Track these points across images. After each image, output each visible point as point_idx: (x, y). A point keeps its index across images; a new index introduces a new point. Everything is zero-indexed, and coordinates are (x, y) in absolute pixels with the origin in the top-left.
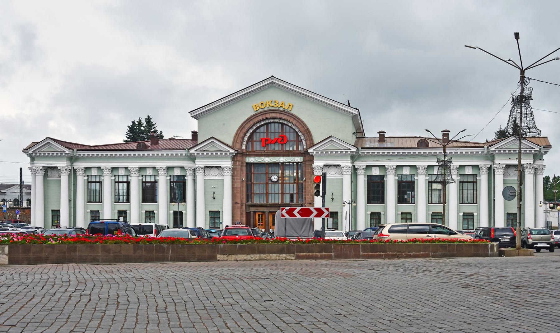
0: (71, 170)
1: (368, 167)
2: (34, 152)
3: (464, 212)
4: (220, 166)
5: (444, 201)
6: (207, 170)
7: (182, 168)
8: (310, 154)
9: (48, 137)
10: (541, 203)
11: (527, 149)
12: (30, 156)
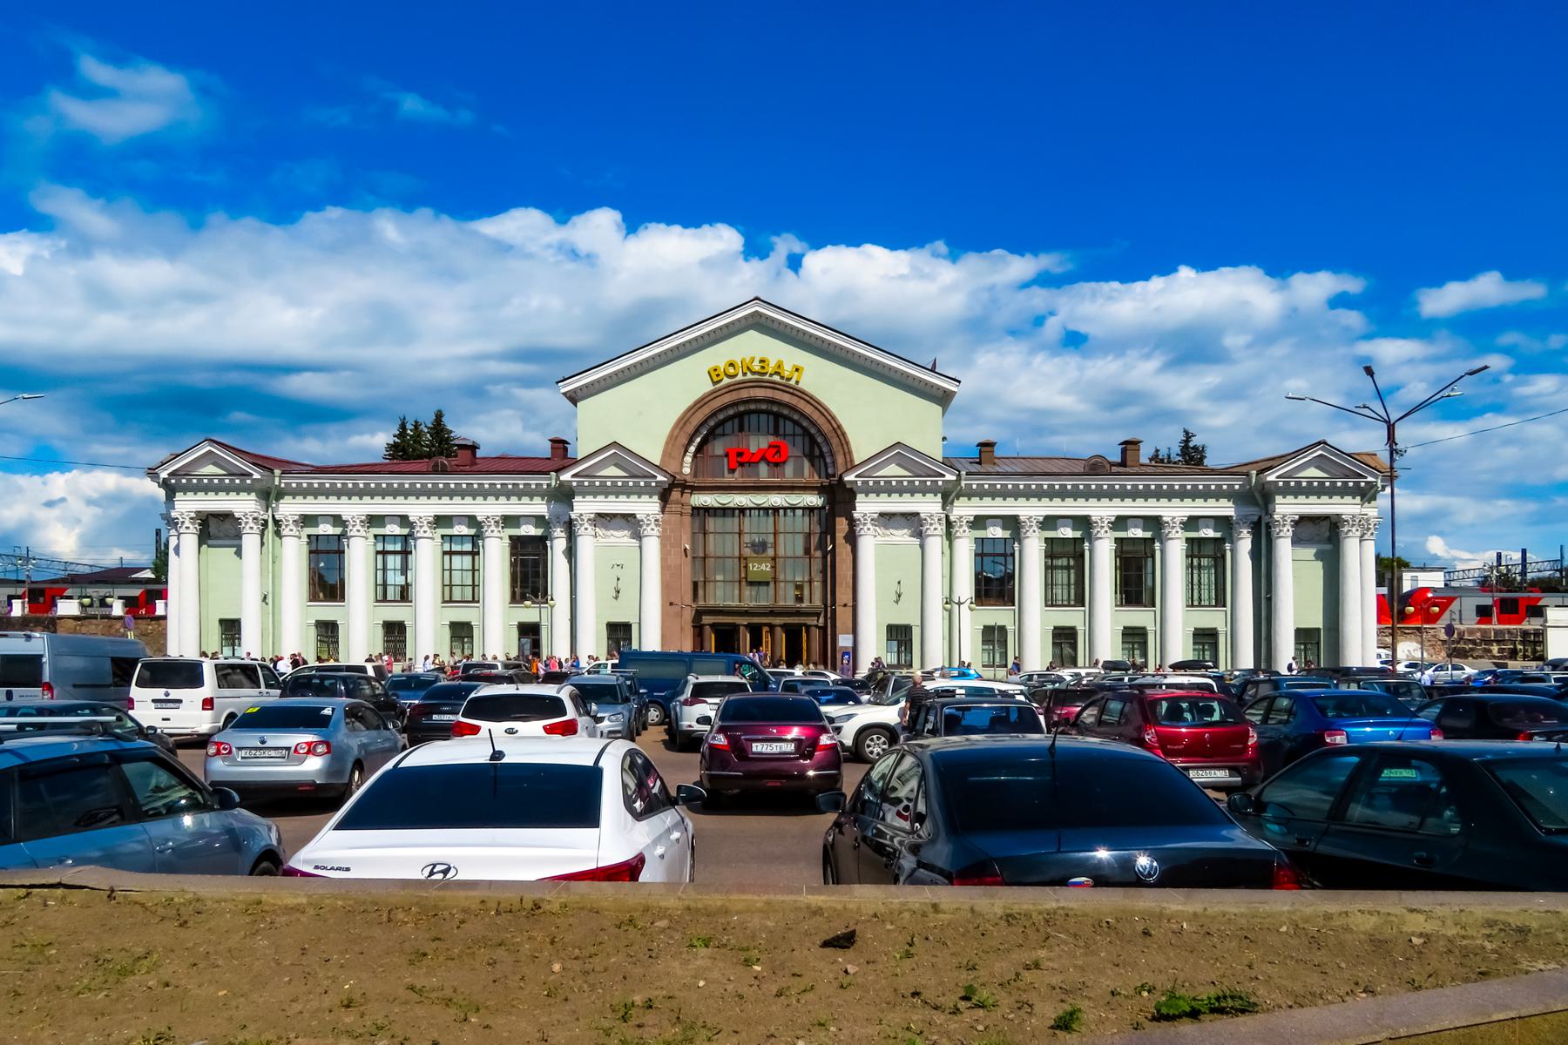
2: (172, 474)
3: (987, 624)
4: (634, 514)
8: (848, 486)
11: (1347, 477)
12: (165, 484)
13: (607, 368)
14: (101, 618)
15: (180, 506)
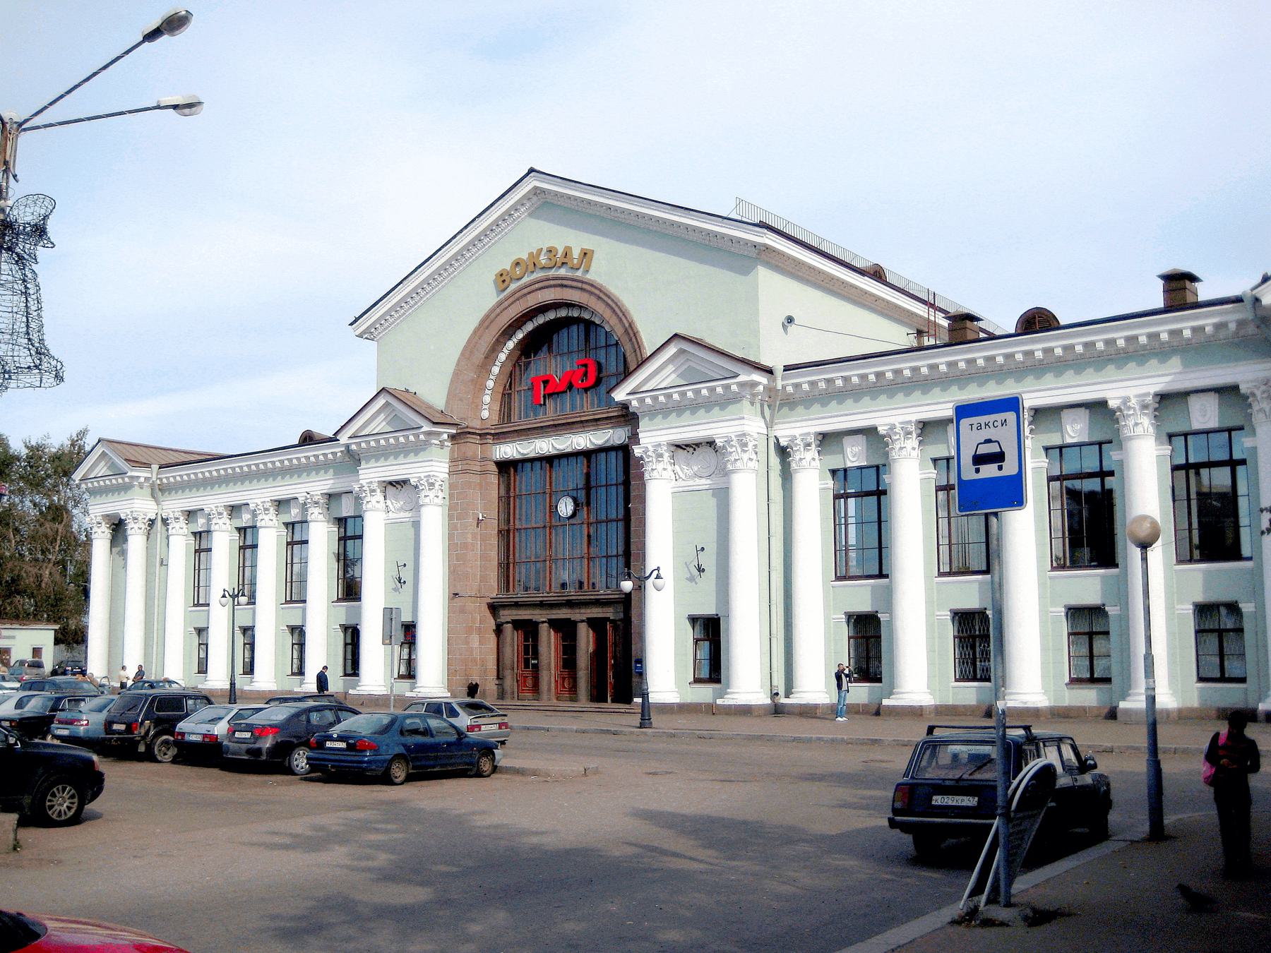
0: (152, 523)
1: (1164, 399)
9: (678, 331)
10: (224, 596)
13: (738, 229)
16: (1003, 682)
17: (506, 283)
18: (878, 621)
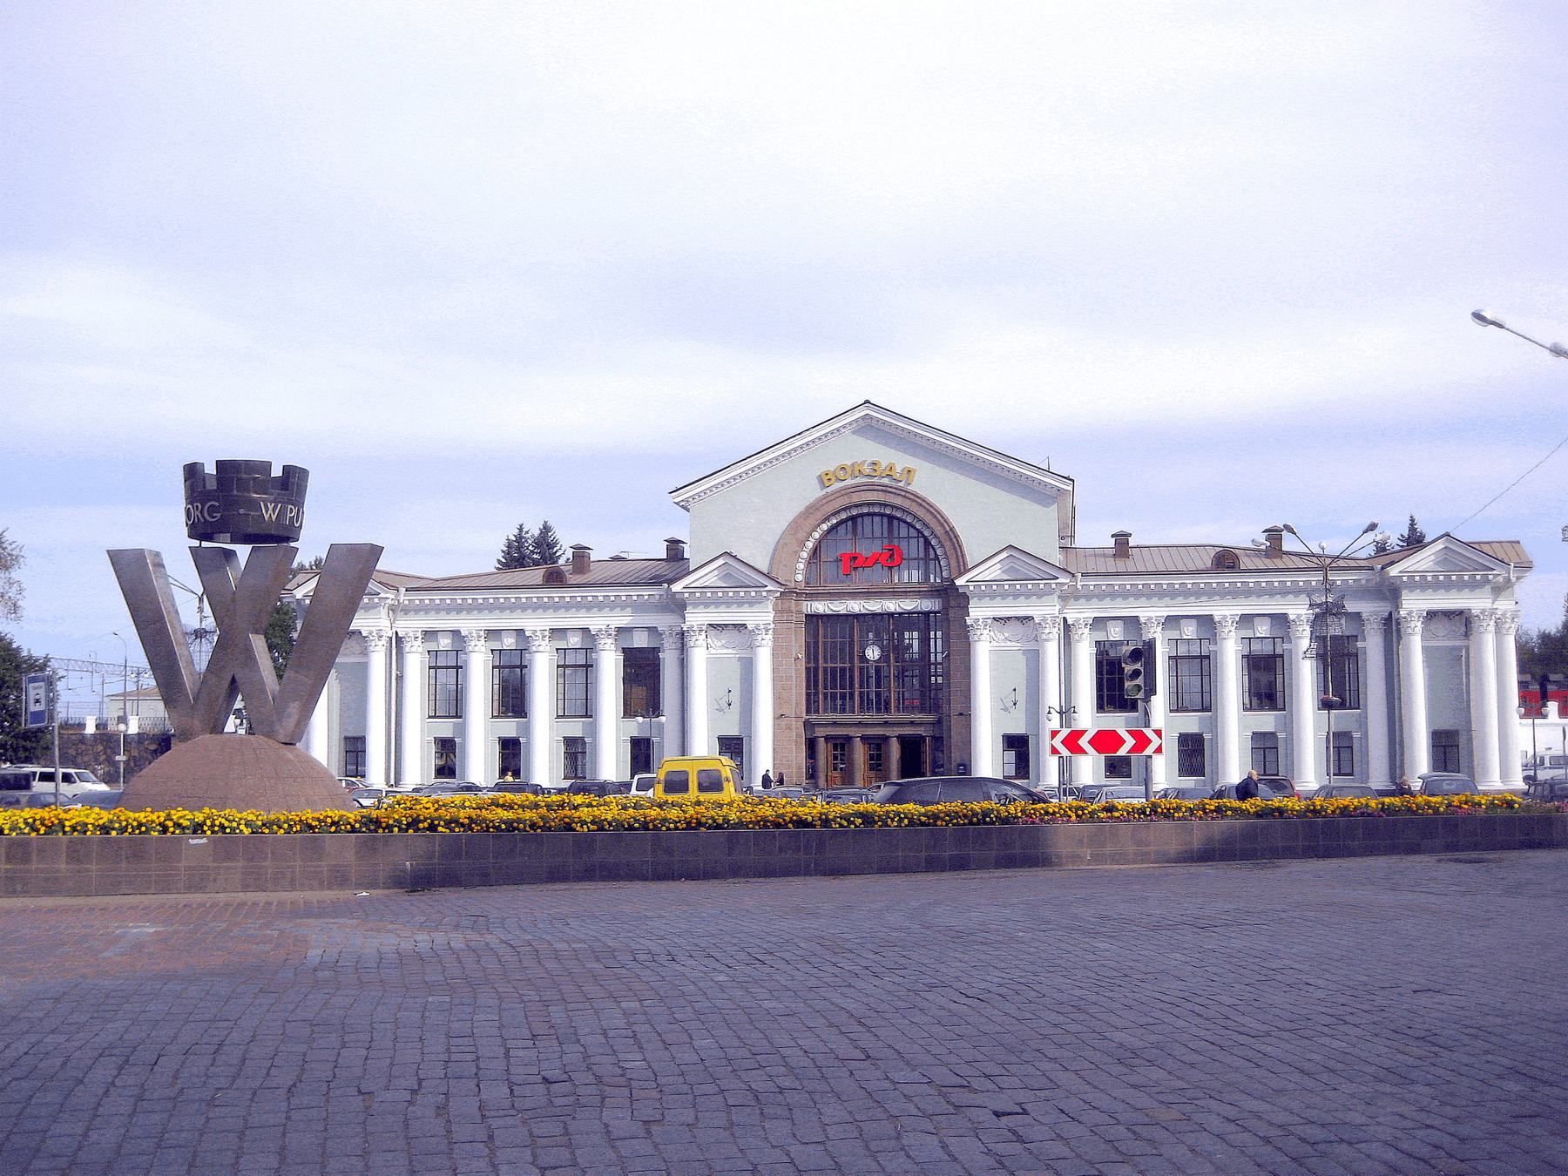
3: (1255, 730)
5: (588, 711)
6: (712, 632)
7: (652, 630)
11: (1477, 570)
14: (844, 750)
15: (974, 614)
16: (1215, 772)
17: (831, 482)
18: (584, 743)
